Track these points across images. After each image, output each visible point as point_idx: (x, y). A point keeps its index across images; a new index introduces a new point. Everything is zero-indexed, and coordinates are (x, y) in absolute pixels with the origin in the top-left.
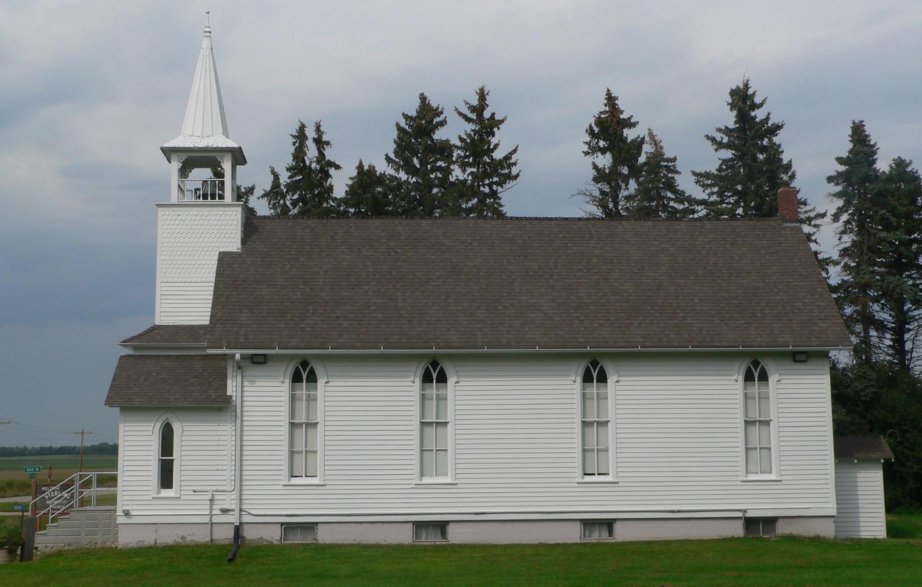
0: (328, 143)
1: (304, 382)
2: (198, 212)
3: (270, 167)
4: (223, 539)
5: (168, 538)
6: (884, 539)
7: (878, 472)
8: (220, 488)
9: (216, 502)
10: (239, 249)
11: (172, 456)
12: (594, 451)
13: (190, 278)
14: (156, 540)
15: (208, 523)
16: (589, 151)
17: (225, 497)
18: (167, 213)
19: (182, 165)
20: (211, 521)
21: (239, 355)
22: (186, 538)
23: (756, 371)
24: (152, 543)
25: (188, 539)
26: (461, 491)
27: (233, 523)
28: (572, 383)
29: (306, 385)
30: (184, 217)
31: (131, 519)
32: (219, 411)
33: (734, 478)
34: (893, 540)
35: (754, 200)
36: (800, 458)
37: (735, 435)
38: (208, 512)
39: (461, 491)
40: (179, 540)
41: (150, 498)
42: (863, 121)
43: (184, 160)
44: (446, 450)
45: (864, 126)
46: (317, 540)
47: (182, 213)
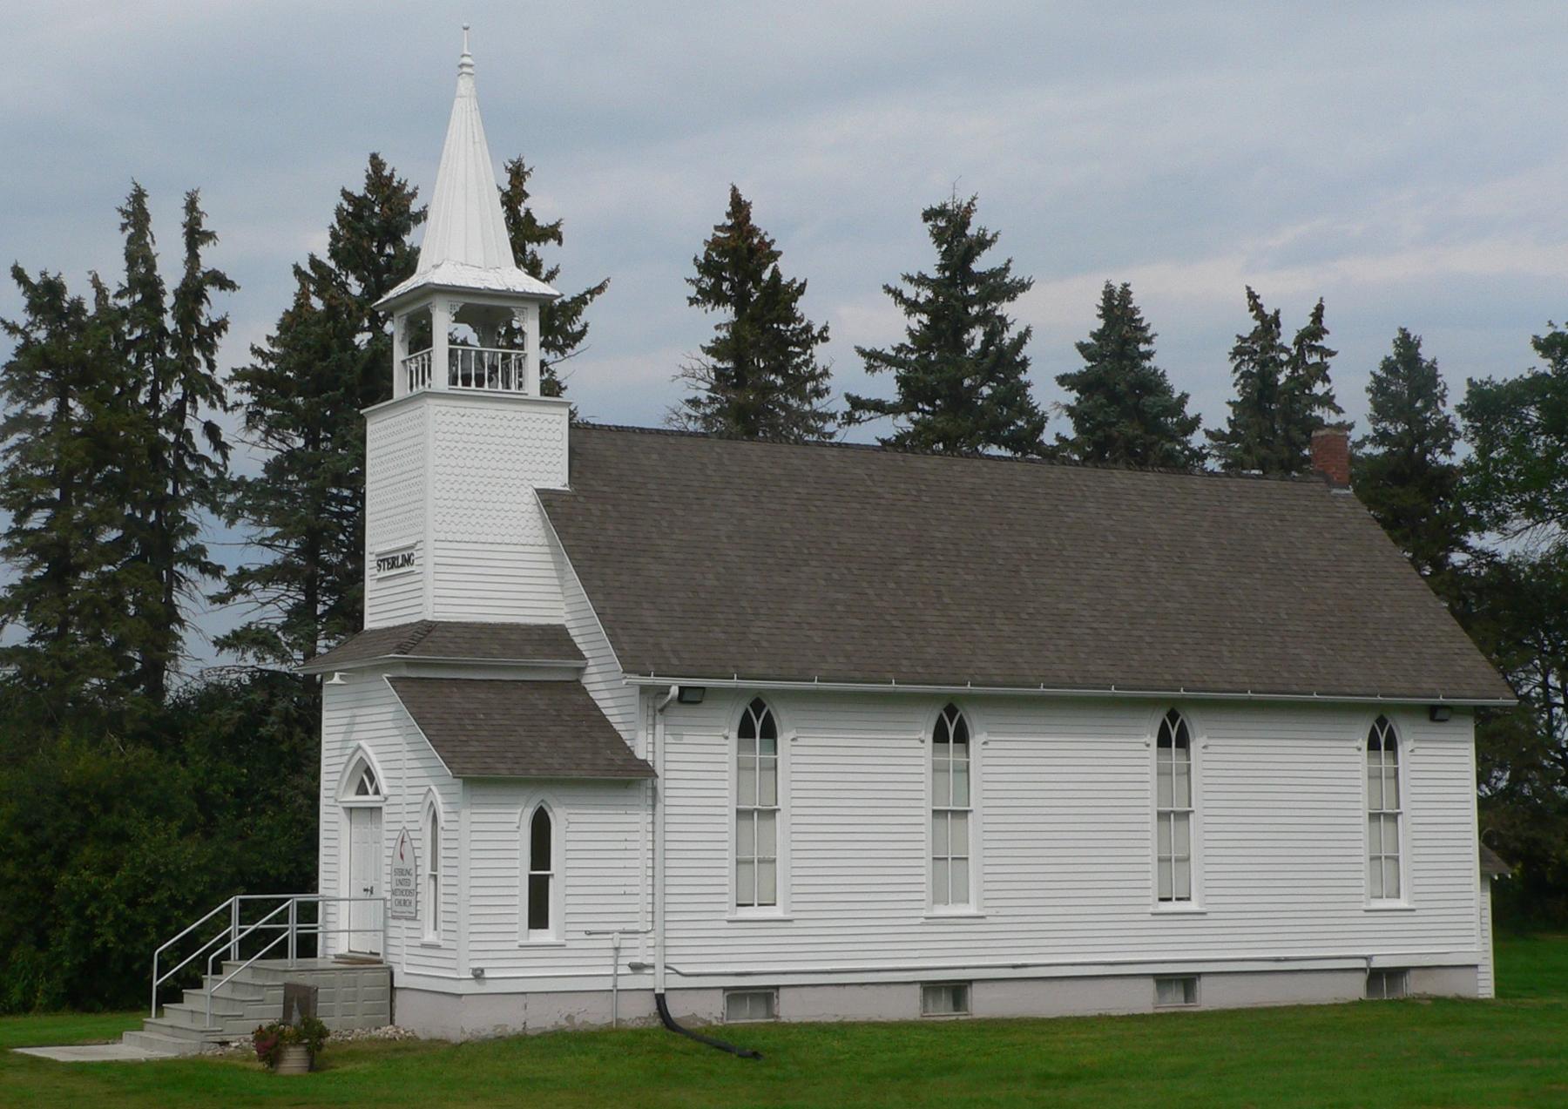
0: (210, 236)
2: (538, 416)
3: (90, 273)
5: (544, 1018)
6: (1491, 999)
8: (629, 927)
9: (623, 953)
10: (565, 485)
11: (549, 869)
12: (753, 862)
13: (459, 534)
15: (611, 991)
16: (699, 296)
17: (636, 943)
18: (444, 409)
20: (615, 986)
21: (677, 688)
22: (573, 1018)
23: (951, 723)
24: (520, 1028)
25: (578, 1020)
27: (653, 990)
29: (760, 742)
30: (473, 421)
31: (484, 984)
34: (1501, 1001)
36: (1042, 877)
38: (611, 972)
40: (563, 1023)
41: (515, 946)
42: (1128, 285)
43: (458, 309)
44: (966, 859)
45: (1131, 293)
46: (777, 1017)
47: (468, 411)
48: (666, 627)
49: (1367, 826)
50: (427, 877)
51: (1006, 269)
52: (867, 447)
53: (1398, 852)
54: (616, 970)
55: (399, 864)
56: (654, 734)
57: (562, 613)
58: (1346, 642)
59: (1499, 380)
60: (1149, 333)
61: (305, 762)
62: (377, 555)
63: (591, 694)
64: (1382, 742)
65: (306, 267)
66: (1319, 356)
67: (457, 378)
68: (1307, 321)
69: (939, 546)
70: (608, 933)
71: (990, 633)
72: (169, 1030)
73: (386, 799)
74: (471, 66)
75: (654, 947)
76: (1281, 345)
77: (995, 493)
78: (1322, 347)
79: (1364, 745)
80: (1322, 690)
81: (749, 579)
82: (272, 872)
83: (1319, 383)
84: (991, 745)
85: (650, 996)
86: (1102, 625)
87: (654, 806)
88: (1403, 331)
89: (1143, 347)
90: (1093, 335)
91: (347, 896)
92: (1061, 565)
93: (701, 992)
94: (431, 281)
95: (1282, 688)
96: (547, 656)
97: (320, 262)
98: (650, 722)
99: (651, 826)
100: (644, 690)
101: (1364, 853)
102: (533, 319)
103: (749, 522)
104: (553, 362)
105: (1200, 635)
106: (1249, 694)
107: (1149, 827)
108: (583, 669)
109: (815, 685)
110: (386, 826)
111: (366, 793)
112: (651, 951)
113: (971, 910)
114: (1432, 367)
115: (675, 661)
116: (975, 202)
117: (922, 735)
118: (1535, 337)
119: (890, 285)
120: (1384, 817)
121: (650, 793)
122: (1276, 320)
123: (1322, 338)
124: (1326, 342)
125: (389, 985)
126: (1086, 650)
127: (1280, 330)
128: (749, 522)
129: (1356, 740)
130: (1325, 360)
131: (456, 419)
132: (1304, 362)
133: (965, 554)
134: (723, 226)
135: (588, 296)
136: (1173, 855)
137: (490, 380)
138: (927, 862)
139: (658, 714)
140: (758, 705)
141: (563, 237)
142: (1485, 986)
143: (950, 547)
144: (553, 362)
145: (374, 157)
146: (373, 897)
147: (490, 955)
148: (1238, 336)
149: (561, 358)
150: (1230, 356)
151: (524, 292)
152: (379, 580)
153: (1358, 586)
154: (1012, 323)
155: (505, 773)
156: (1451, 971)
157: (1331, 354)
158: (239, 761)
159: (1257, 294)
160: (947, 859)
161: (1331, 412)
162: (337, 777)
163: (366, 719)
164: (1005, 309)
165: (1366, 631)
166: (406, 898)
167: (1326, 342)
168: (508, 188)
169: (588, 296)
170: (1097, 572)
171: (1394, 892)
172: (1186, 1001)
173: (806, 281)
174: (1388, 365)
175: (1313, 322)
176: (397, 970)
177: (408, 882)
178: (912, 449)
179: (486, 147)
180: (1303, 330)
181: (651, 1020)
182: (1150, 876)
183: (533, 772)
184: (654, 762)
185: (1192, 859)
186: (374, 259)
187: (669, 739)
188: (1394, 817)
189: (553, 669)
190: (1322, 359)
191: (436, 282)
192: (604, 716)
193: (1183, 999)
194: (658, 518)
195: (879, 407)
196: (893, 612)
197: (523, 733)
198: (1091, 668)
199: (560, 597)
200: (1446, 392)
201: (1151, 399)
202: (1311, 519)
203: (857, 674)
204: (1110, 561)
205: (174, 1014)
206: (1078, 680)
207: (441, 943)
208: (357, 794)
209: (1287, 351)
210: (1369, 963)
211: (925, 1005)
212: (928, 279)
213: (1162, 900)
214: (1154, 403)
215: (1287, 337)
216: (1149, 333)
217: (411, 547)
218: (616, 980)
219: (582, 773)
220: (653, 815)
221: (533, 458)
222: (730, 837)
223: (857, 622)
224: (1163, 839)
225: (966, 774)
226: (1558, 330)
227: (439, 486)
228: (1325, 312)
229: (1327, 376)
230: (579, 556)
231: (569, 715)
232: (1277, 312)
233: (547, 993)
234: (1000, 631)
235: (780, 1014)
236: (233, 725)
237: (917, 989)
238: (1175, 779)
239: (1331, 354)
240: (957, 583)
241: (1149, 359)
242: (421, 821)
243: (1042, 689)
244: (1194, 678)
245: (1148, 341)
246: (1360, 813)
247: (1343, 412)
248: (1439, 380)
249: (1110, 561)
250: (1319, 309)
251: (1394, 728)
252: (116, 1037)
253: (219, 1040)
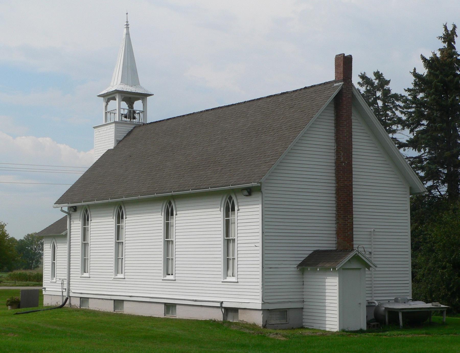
7: (336, 278)
156: (252, 311)
233: (54, 295)
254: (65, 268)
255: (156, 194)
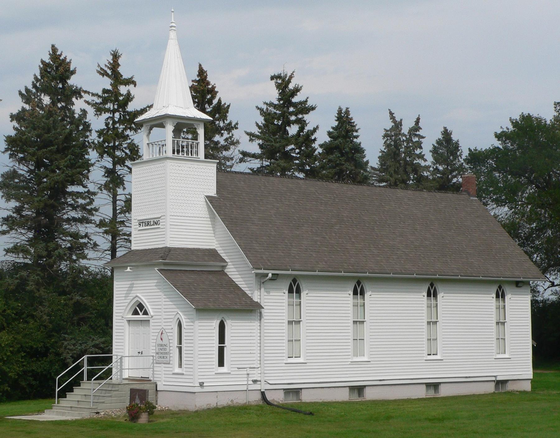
1: (295, 293)
2: (206, 167)
4: (253, 401)
5: (223, 401)
8: (252, 366)
9: (250, 376)
10: (215, 194)
14: (217, 403)
15: (246, 390)
19: (174, 128)
20: (247, 389)
22: (233, 401)
24: (215, 405)
25: (235, 402)
26: (373, 366)
27: (260, 390)
28: (422, 297)
31: (204, 388)
32: (251, 312)
33: (420, 358)
35: (113, 133)
37: (491, 331)
39: (373, 366)
40: (230, 403)
42: (348, 108)
43: (175, 124)
44: (363, 339)
46: (301, 400)
48: (263, 251)
49: (495, 327)
50: (176, 347)
51: (306, 101)
52: (246, 173)
53: (505, 336)
54: (248, 383)
55: (160, 342)
56: (260, 292)
57: (214, 244)
58: (487, 257)
59: (479, 149)
60: (357, 128)
61: (44, 301)
62: (138, 221)
63: (229, 276)
64: (500, 295)
65: (24, 92)
66: (418, 138)
67: (175, 151)
68: (413, 124)
69: (345, 219)
70: (245, 368)
71: (370, 253)
72: (69, 409)
73: (152, 317)
74: (175, 27)
75: (261, 373)
76: (403, 133)
77: (360, 198)
78: (419, 135)
79: (426, 295)
80: (483, 275)
81: (286, 231)
82: (35, 346)
83: (419, 149)
84: (444, 298)
85: (259, 393)
86: (406, 250)
87: (260, 320)
88: (445, 128)
89: (355, 134)
90: (333, 128)
91: (128, 355)
92: (388, 226)
93: (276, 391)
94: (167, 113)
95: (470, 275)
96: (213, 261)
97: (29, 90)
98: (259, 287)
99: (259, 327)
100: (257, 275)
101: (494, 336)
102: (202, 129)
103: (280, 209)
104: (131, 135)
105: (439, 254)
106: (459, 277)
107: (424, 327)
108: (226, 266)
109: (317, 273)
110: (152, 327)
111: (139, 314)
112: (259, 375)
113: (365, 359)
114: (457, 143)
115: (269, 264)
116: (294, 73)
117: (285, 291)
118: (496, 132)
119: (259, 106)
120: (501, 323)
121: (259, 315)
122: (400, 123)
123: (419, 131)
124: (420, 133)
125: (155, 390)
126: (403, 260)
127: (402, 127)
128: (280, 209)
129: (492, 294)
130: (420, 140)
131: (177, 168)
132: (412, 141)
133: (355, 222)
134: (195, 80)
135: (148, 109)
136: (500, 337)
137: (182, 151)
138: (351, 341)
139: (262, 284)
140: (294, 281)
141: (137, 83)
142: (527, 387)
143: (350, 219)
144: (131, 135)
145: (53, 46)
146: (142, 355)
147: (205, 377)
148: (385, 129)
149: (135, 133)
150: (383, 137)
151: (200, 118)
152: (139, 230)
153: (486, 235)
154: (308, 123)
155: (212, 307)
156: (518, 381)
157: (423, 137)
158: (17, 300)
159: (393, 112)
160: (357, 339)
161: (422, 161)
162: (124, 308)
163: (137, 285)
164: (307, 117)
165: (492, 253)
166: (164, 355)
167: (420, 133)
168: (112, 62)
169: (148, 109)
170: (400, 230)
171: (503, 352)
172: (435, 393)
173: (230, 104)
174: (439, 142)
175: (415, 124)
176: (158, 383)
177: (165, 349)
178: (267, 175)
179: (181, 60)
180: (412, 128)
181: (259, 402)
182: (424, 346)
183: (221, 306)
184: (260, 302)
185: (438, 339)
186: (57, 90)
187: (266, 294)
188: (503, 323)
189: (214, 266)
190: (419, 139)
191: (170, 114)
192: (237, 284)
193: (434, 392)
194: (249, 207)
195: (254, 156)
196: (337, 245)
197: (212, 291)
198: (406, 267)
199: (214, 238)
200: (462, 153)
201: (359, 155)
202: (466, 209)
203: (330, 269)
204: (403, 225)
205: (64, 402)
206: (403, 272)
207: (184, 373)
208: (133, 314)
209: (405, 136)
210: (496, 379)
211: (350, 395)
212: (274, 104)
213: (428, 355)
214: (360, 156)
215: (405, 130)
216: (357, 128)
217: (159, 218)
218: (247, 386)
219: (238, 307)
220: (260, 323)
221: (192, 182)
222: (286, 331)
223: (326, 249)
224: (355, 332)
225: (430, 308)
226: (504, 130)
227: (172, 194)
228: (420, 121)
229: (421, 146)
230: (227, 223)
231: (225, 284)
232: (401, 120)
233: (224, 391)
234: (373, 252)
235: (302, 399)
236: (14, 285)
237: (348, 389)
238: (433, 308)
239: (423, 137)
240: (355, 234)
241: (357, 138)
242: (172, 326)
243: (368, 274)
244: (441, 271)
245: (357, 131)
246: (493, 322)
247: (427, 161)
248: (459, 148)
249: (403, 225)
250: (418, 119)
251: (300, 284)
252: (40, 411)
253: (96, 412)
254: (251, 353)
255: (416, 275)
